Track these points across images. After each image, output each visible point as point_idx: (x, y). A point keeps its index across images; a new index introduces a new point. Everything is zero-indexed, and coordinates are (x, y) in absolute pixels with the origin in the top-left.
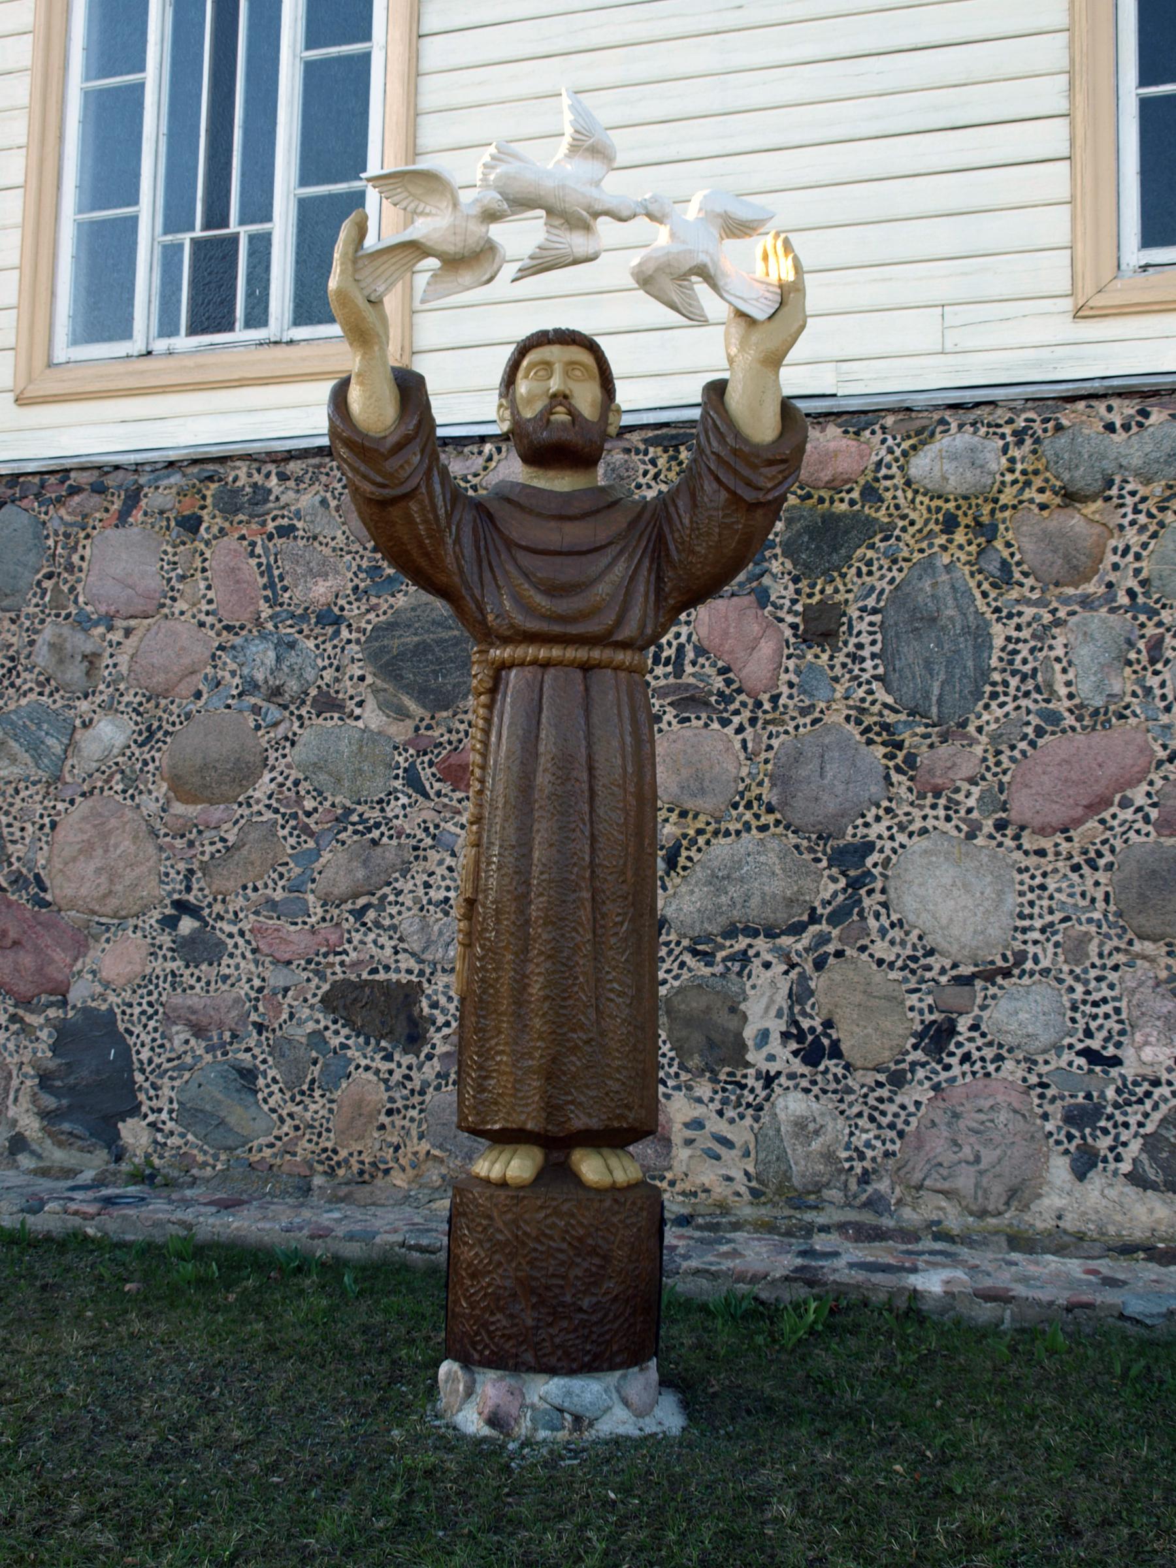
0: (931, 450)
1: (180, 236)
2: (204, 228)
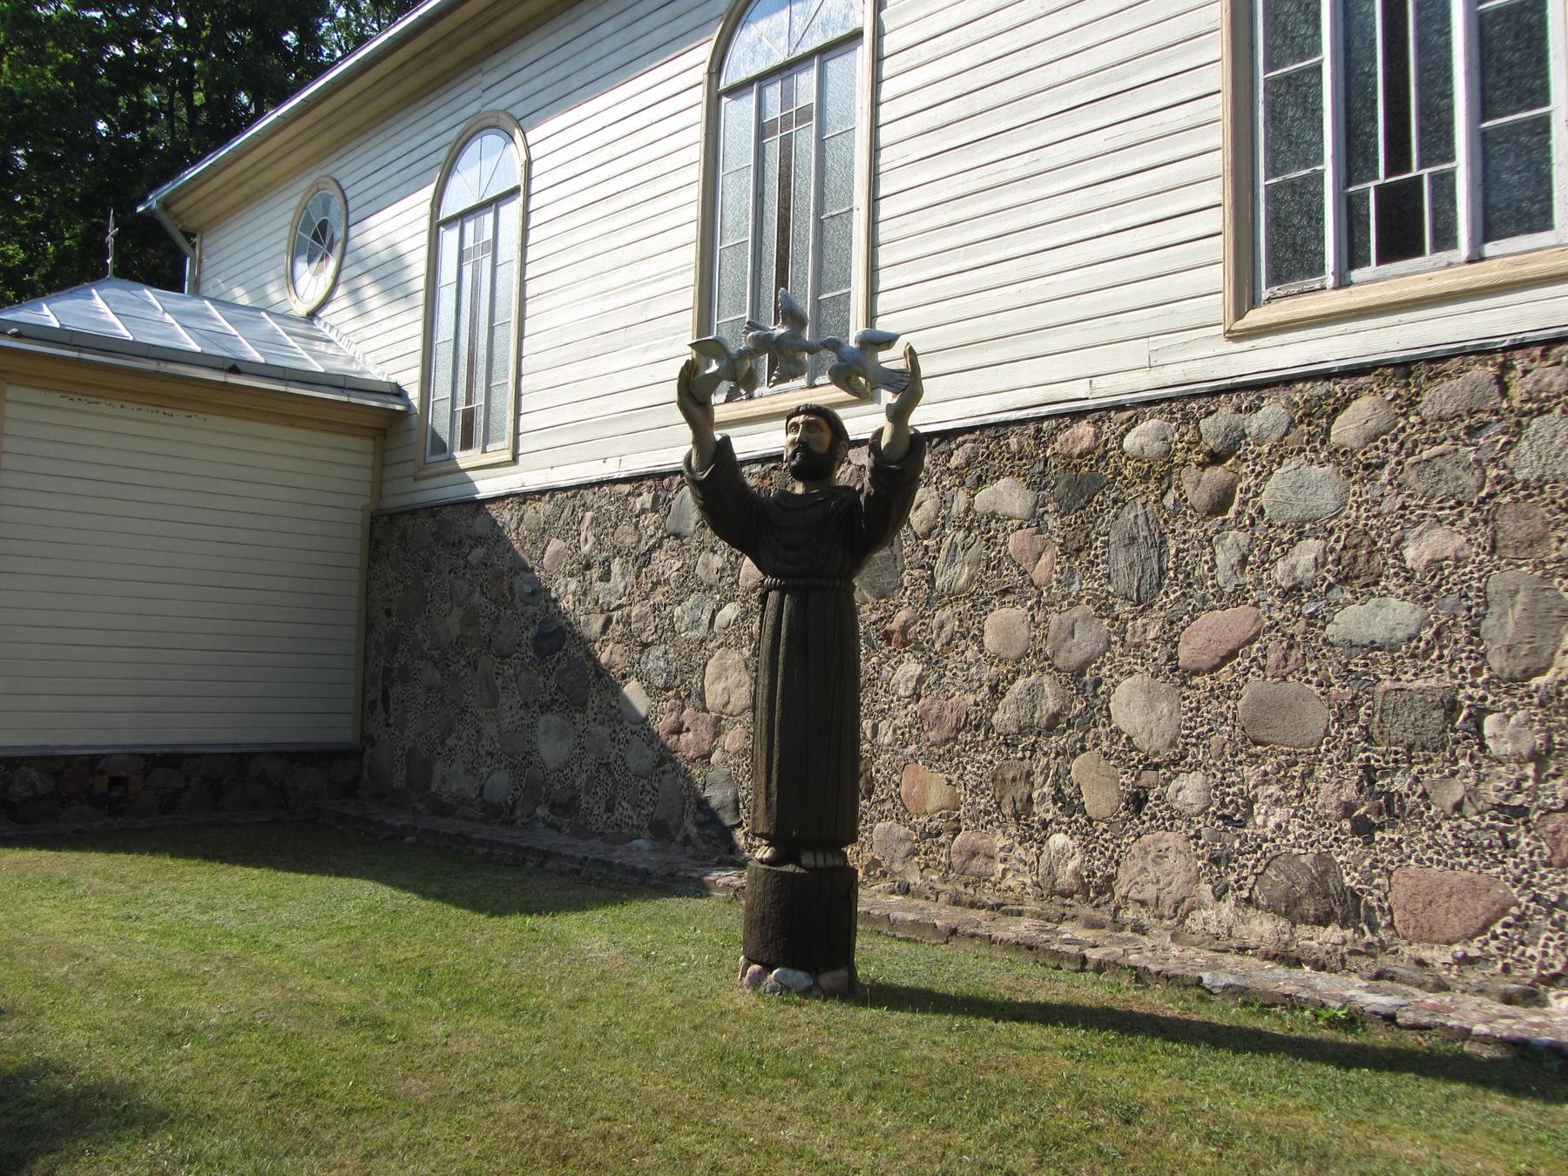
0: (1134, 432)
1: (1365, 186)
2: (1387, 176)
